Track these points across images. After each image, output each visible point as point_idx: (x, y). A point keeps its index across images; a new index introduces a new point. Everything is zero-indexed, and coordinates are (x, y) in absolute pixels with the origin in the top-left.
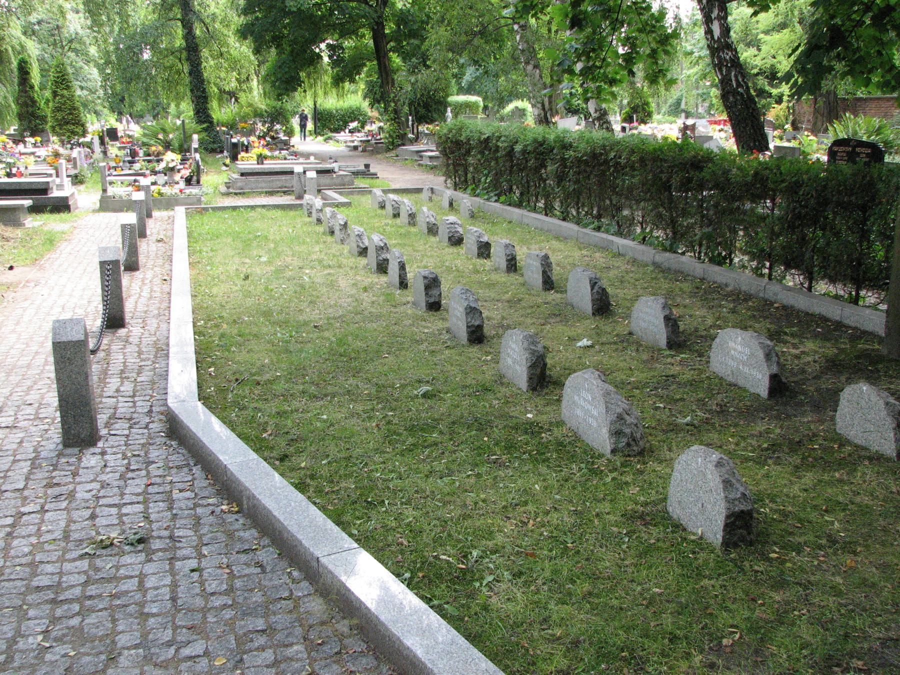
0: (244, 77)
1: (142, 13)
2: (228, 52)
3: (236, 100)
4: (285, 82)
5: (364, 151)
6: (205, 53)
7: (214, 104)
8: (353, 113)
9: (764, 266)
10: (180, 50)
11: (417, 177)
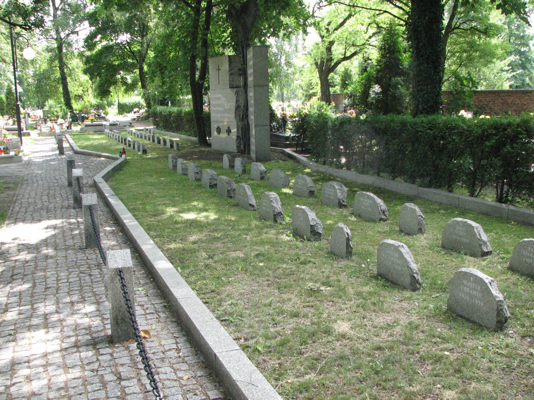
0: (86, 89)
1: (69, 361)
3: (83, 99)
4: (103, 92)
5: (138, 120)
6: (69, 79)
8: (136, 104)
9: (123, 79)
10: (58, 79)
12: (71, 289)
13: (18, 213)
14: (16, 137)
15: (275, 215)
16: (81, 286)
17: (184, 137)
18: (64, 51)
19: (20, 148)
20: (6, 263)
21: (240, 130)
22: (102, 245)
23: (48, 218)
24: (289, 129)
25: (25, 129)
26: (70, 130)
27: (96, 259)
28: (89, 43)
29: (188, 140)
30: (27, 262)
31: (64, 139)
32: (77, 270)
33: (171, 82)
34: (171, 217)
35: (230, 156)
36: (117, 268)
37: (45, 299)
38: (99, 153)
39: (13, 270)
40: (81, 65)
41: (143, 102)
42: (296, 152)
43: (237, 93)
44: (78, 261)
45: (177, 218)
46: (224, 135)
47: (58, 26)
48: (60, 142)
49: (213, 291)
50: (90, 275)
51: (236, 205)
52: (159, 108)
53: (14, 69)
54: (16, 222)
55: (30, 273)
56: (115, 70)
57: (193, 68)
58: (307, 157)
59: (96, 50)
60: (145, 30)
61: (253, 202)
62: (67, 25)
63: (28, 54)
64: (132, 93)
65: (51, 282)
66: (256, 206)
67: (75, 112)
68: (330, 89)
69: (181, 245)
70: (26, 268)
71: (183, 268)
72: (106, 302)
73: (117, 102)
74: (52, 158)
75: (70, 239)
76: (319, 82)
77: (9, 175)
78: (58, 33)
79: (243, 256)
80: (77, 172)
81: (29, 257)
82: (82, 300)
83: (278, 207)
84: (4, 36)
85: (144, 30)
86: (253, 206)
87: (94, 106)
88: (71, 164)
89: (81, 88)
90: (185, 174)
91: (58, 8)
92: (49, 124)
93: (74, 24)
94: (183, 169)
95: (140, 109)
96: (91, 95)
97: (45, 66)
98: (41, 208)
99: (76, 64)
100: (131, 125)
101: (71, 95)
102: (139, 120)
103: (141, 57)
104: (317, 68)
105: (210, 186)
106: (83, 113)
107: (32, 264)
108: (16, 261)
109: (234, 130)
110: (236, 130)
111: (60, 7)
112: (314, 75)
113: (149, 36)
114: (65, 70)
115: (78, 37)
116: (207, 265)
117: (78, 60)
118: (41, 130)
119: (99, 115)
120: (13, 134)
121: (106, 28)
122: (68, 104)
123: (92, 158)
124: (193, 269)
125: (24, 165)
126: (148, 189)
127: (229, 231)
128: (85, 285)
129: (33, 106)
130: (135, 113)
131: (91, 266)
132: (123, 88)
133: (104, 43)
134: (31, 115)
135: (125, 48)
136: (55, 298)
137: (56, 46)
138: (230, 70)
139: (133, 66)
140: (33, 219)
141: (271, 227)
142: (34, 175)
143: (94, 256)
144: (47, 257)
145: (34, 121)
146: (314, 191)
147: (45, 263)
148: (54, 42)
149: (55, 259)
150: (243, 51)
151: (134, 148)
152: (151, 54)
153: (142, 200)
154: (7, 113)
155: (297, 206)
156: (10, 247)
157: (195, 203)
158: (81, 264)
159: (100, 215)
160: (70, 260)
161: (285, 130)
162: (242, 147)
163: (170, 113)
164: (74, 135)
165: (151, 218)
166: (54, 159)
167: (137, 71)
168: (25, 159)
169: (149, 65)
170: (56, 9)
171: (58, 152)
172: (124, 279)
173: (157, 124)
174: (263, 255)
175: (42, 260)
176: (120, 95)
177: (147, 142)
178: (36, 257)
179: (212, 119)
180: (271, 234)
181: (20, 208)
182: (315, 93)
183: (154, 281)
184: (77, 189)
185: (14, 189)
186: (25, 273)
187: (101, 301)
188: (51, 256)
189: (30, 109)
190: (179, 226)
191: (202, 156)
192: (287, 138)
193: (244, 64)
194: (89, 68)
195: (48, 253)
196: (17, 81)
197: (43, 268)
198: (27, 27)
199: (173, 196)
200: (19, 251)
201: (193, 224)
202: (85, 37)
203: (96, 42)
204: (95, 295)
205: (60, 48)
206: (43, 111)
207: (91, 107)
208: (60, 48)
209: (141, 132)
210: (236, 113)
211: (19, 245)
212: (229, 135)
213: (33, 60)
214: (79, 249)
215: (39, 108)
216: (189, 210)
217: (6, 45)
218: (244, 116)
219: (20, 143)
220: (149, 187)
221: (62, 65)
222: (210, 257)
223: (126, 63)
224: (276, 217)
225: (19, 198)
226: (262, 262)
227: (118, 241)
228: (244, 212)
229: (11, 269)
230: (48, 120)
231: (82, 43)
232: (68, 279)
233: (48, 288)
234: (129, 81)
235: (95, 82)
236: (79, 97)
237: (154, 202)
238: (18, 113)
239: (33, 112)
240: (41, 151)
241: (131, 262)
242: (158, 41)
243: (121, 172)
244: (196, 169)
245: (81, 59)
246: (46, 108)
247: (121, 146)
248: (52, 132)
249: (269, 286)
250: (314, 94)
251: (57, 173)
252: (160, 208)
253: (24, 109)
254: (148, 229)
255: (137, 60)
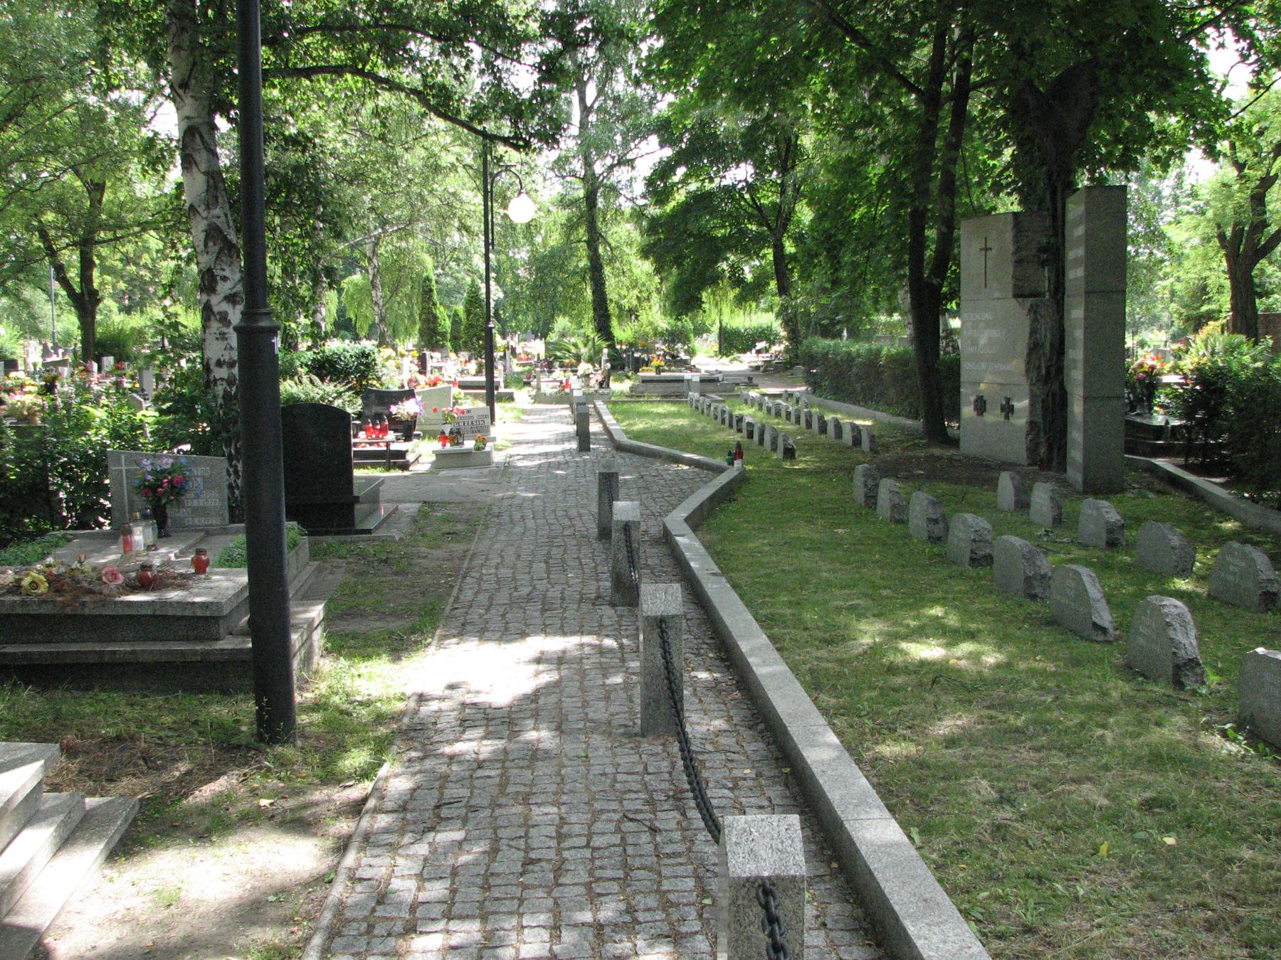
0: (645, 295)
2: (630, 270)
3: (637, 317)
4: (685, 300)
6: (607, 270)
7: (614, 322)
8: (763, 331)
10: (584, 270)
11: (894, 420)
12: (598, 873)
13: (470, 606)
14: (481, 404)
15: (1178, 668)
16: (626, 866)
17: (885, 417)
18: (600, 203)
19: (488, 431)
20: (428, 764)
21: (1039, 406)
22: (688, 729)
23: (545, 630)
24: (1162, 406)
25: (502, 384)
26: (606, 391)
27: (670, 773)
28: (656, 188)
29: (895, 427)
30: (480, 765)
31: (592, 411)
32: (614, 806)
33: (854, 283)
34: (874, 650)
35: (1017, 477)
36: (758, 877)
37: (521, 901)
38: (678, 452)
39: (442, 787)
40: (636, 236)
41: (777, 326)
42: (1185, 467)
43: (1033, 310)
44: (620, 777)
45: (892, 657)
46: (993, 416)
47: (590, 147)
48: (582, 420)
49: (1029, 930)
50: (654, 830)
51: (1052, 622)
52: (822, 344)
53: (487, 244)
54: (462, 633)
55: (486, 803)
56: (716, 249)
57: (919, 242)
58: (1221, 485)
59: (672, 204)
60: (791, 155)
61: (1105, 617)
62: (610, 145)
63: (520, 211)
64: (754, 305)
65: (542, 840)
66: (1111, 631)
67: (618, 347)
68: (1257, 301)
69: (912, 749)
70: (476, 783)
71: (926, 830)
72: (700, 937)
73: (718, 324)
74: (560, 458)
75: (600, 699)
76: (1228, 283)
77: (458, 499)
78: (588, 164)
79: (1106, 802)
80: (624, 509)
81: (487, 748)
82: (627, 918)
83: (1186, 642)
84: (471, 172)
85: (788, 154)
86: (1103, 630)
87: (662, 334)
88: (608, 485)
89: (636, 292)
90: (898, 522)
91: (592, 106)
92: (558, 374)
93: (625, 143)
94: (894, 507)
95: (772, 343)
96: (656, 308)
97: (555, 240)
98: (529, 598)
99: (623, 234)
100: (750, 384)
101: (612, 308)
102: (770, 370)
103: (780, 219)
104: (1223, 246)
105: (972, 559)
106: (637, 351)
107: (493, 773)
108: (452, 757)
109: (1022, 404)
110: (1026, 402)
111: (596, 106)
112: (1214, 265)
113: (799, 170)
114: (601, 250)
115: (634, 174)
116: (999, 827)
117: (630, 226)
118: (539, 389)
119: (673, 357)
120: (476, 396)
121: (701, 149)
122: (604, 329)
123: (658, 465)
124: (956, 837)
125: (496, 473)
126: (806, 559)
127: (1048, 709)
128: (637, 864)
129: (525, 331)
130: (758, 352)
131: (655, 796)
132: (732, 294)
133: (693, 186)
134: (518, 351)
135: (742, 197)
136: (550, 902)
137: (581, 193)
138: (1018, 250)
139: (760, 240)
140: (506, 629)
141: (1170, 703)
142: (516, 502)
143: (665, 764)
144: (534, 755)
145: (524, 365)
146: (1275, 594)
147: (528, 773)
148: (578, 184)
149: (555, 762)
150: (1054, 200)
151: (761, 441)
152: (805, 214)
153: (791, 592)
154: (466, 346)
155: (1261, 650)
156: (440, 711)
157: (937, 611)
158: (628, 786)
159: (685, 641)
160: (596, 770)
161: (1151, 409)
162: (1042, 450)
163: (850, 358)
164: (615, 403)
165: (818, 648)
166: (567, 463)
167: (769, 253)
168: (498, 457)
169: (799, 239)
170: (586, 110)
171: (574, 445)
172: (777, 920)
173: (815, 384)
174: (1168, 805)
175: (522, 763)
176: (726, 310)
177: (791, 427)
178: (505, 751)
179: (964, 377)
180: (1172, 730)
181: (476, 593)
182: (1213, 311)
183: (842, 869)
184: (623, 554)
185: (467, 537)
186: (473, 802)
187: (684, 929)
188: (546, 751)
189: (516, 339)
190: (899, 680)
191: (934, 473)
192: (1159, 431)
193: (1056, 235)
194: (655, 244)
195: (539, 740)
196: (493, 275)
197: (522, 789)
198: (521, 143)
199: (874, 586)
200: (464, 724)
201: (936, 678)
202: (648, 173)
203: (675, 184)
204: (667, 905)
205: (591, 198)
206: (547, 344)
207: (655, 335)
208: (591, 198)
209: (779, 401)
210: (1028, 363)
211: (464, 705)
212: (1007, 417)
213: (528, 226)
214: (623, 735)
215: (536, 337)
216: (919, 634)
217: (471, 194)
218: (1053, 371)
219: (488, 421)
220: (806, 553)
221: (595, 238)
222: (1004, 799)
223: (743, 232)
224: (1182, 672)
225: (475, 563)
226: (1167, 830)
227: (730, 719)
228: (1082, 648)
229: (437, 784)
230: (556, 364)
231: (640, 188)
232: (590, 836)
233: (533, 862)
234: (749, 277)
235: (666, 279)
236: (632, 313)
237: (825, 602)
238: (490, 347)
239: (522, 344)
240: (535, 442)
241: (801, 858)
242: (823, 178)
243: (733, 506)
244: (931, 510)
245: (638, 223)
246: (553, 337)
247: (733, 437)
248: (563, 397)
249: (1210, 927)
250: (1210, 316)
251: (572, 500)
252: (841, 619)
253: (504, 338)
254: (815, 684)
255: (768, 226)
